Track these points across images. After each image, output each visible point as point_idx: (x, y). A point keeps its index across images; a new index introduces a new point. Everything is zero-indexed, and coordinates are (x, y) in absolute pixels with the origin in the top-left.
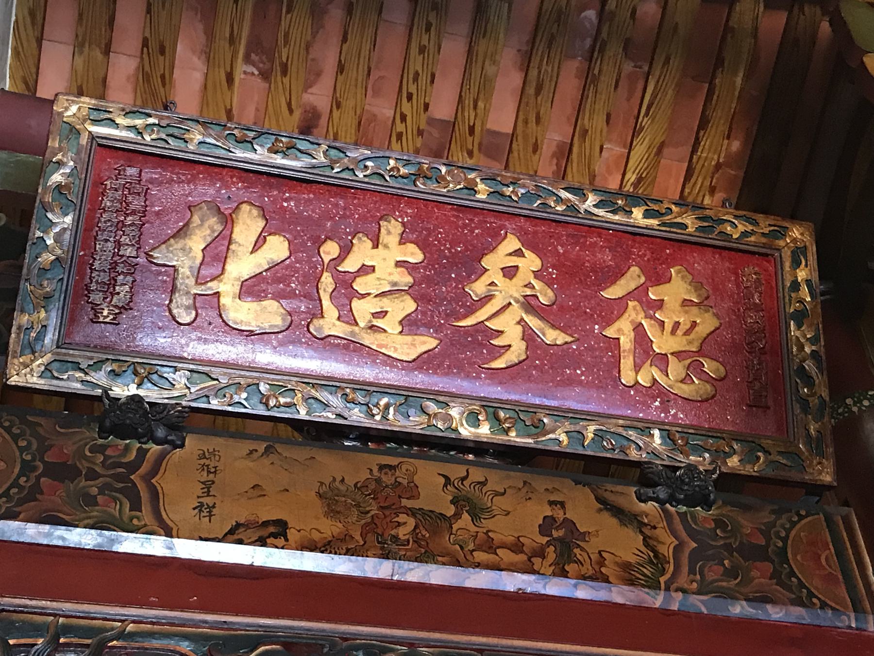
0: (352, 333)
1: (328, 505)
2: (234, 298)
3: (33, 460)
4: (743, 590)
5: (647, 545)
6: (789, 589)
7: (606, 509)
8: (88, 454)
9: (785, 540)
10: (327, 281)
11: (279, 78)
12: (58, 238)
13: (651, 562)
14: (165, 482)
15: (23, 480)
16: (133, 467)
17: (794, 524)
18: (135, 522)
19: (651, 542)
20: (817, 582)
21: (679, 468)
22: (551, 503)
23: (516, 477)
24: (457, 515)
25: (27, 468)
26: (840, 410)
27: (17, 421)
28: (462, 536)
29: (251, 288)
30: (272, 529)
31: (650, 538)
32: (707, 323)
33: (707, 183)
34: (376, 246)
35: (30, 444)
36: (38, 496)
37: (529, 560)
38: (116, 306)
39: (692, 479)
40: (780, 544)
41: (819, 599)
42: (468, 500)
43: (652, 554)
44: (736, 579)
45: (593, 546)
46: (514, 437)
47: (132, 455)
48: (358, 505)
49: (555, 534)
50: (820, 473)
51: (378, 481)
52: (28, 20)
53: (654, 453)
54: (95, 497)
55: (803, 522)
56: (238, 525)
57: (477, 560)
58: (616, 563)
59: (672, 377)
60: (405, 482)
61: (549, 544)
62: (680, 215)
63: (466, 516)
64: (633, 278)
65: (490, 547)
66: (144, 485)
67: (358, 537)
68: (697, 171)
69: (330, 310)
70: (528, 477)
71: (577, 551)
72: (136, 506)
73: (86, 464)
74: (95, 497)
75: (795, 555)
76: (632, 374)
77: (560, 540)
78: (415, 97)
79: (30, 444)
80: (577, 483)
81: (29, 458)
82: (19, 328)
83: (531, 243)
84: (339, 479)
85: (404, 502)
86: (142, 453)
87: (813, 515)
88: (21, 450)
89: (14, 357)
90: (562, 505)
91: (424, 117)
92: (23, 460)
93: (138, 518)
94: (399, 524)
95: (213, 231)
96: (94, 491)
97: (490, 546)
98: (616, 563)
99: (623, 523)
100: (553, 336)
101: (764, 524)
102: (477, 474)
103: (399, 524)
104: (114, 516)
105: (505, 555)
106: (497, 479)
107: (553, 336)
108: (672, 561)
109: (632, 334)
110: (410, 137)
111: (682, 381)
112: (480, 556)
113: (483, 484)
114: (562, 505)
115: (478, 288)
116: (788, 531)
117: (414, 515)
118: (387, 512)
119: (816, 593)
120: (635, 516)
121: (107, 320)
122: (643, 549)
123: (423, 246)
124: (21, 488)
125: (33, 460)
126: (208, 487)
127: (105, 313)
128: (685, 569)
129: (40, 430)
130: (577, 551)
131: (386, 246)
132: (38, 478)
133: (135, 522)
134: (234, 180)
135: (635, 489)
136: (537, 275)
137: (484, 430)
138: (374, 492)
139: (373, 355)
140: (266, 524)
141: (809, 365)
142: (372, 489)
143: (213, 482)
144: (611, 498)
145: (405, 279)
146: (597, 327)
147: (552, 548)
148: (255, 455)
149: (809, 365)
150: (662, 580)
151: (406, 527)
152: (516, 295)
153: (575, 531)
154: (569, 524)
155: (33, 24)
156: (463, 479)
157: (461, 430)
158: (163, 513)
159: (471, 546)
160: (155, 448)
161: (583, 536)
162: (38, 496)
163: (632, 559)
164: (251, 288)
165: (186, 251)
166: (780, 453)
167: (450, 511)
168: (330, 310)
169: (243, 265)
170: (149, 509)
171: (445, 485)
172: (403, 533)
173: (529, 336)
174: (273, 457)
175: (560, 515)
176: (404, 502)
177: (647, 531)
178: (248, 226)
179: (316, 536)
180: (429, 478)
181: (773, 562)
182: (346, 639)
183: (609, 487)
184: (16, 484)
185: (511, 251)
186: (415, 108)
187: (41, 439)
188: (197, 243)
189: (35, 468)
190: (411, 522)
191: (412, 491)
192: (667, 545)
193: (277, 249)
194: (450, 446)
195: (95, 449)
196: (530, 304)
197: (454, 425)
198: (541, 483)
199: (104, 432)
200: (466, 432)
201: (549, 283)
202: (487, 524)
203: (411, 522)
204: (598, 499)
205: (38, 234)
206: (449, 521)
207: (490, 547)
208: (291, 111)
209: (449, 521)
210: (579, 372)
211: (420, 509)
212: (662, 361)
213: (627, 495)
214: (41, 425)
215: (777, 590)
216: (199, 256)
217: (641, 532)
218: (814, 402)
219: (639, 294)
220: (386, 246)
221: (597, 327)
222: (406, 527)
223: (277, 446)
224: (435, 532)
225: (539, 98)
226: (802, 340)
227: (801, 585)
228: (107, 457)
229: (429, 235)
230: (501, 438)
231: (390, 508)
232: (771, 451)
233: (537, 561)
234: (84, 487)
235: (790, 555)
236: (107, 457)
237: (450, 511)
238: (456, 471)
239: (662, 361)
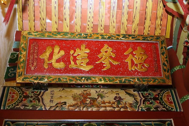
0: (77, 67)
1: (74, 98)
2: (55, 63)
3: (21, 95)
4: (153, 106)
5: (135, 99)
6: (162, 105)
7: (127, 94)
8: (31, 93)
9: (162, 96)
10: (72, 58)
11: (65, 21)
12: (23, 56)
13: (136, 103)
14: (44, 97)
15: (20, 99)
16: (39, 95)
17: (164, 93)
18: (39, 104)
19: (136, 99)
20: (168, 103)
21: (141, 85)
22: (116, 94)
23: (110, 90)
24: (98, 98)
25: (20, 97)
26: (174, 70)
27: (19, 89)
28: (99, 102)
29: (58, 61)
30: (63, 104)
31: (135, 98)
32: (144, 57)
33: (148, 30)
34: (80, 50)
35: (21, 92)
36: (22, 101)
37: (112, 105)
38: (34, 67)
39: (143, 87)
40: (161, 97)
41: (168, 106)
42: (100, 95)
43: (136, 101)
44: (152, 104)
45: (124, 101)
46: (109, 83)
47: (39, 93)
48: (79, 98)
49: (117, 99)
50: (168, 83)
51: (83, 93)
52: (20, 17)
53: (136, 83)
54: (32, 101)
55: (166, 92)
56: (57, 103)
57: (102, 106)
58: (129, 104)
59: (138, 68)
60: (88, 93)
61: (116, 101)
62: (139, 37)
63: (100, 98)
64: (130, 50)
65: (104, 103)
66: (41, 98)
67: (79, 103)
68: (145, 28)
69: (72, 63)
70: (112, 89)
71: (121, 102)
72: (39, 102)
73: (31, 95)
74: (32, 101)
75: (164, 99)
76: (131, 68)
77: (118, 100)
78: (90, 21)
79: (21, 92)
80: (122, 89)
81: (21, 95)
82: (18, 72)
83: (110, 46)
84: (76, 94)
85: (88, 97)
86: (40, 92)
87: (168, 91)
88: (20, 94)
89: (17, 78)
90: (119, 94)
91: (92, 25)
92: (20, 95)
93: (39, 104)
94: (87, 101)
95: (50, 51)
96: (32, 100)
97: (104, 103)
98: (129, 104)
99: (130, 96)
100: (115, 63)
101: (158, 93)
102: (102, 90)
103: (87, 101)
104: (35, 104)
105: (107, 104)
106: (106, 91)
107: (115, 63)
108: (140, 102)
109: (131, 61)
110: (90, 28)
111: (141, 68)
112: (102, 105)
113: (103, 92)
114: (119, 94)
115: (99, 56)
116: (163, 94)
117: (90, 99)
118: (85, 99)
119: (168, 105)
120: (133, 95)
121: (33, 69)
122: (134, 101)
123: (89, 49)
124: (19, 100)
125: (21, 95)
126: (52, 97)
127: (32, 68)
128: (142, 103)
129: (22, 90)
130: (121, 102)
131: (82, 50)
132: (22, 98)
133: (39, 104)
134: (54, 41)
135: (133, 90)
136: (112, 52)
137: (103, 82)
138: (83, 95)
139: (81, 72)
140: (62, 103)
141: (165, 63)
142: (83, 95)
143: (53, 96)
144: (128, 91)
145: (86, 55)
146: (124, 60)
147: (116, 102)
148: (61, 91)
149: (165, 63)
150: (137, 106)
151: (88, 101)
152: (108, 56)
153: (121, 98)
154: (120, 98)
155: (21, 18)
156: (100, 91)
157: (99, 82)
158: (44, 102)
159: (101, 103)
160: (43, 91)
161: (122, 99)
162: (22, 101)
163: (132, 103)
164: (58, 61)
165: (46, 55)
166: (160, 80)
167: (97, 97)
168: (72, 63)
169: (56, 57)
170: (42, 102)
171: (96, 93)
172: (88, 102)
173: (111, 63)
174: (64, 91)
175: (118, 96)
176: (88, 97)
177: (135, 97)
178: (57, 49)
179: (71, 104)
180: (93, 92)
181: (160, 100)
182: (78, 122)
183: (128, 90)
184: (18, 100)
185: (130, 52)
186: (90, 23)
187: (23, 92)
188: (48, 54)
189: (22, 97)
190: (89, 100)
191: (90, 94)
192: (139, 99)
193: (62, 53)
194: (97, 86)
195: (32, 92)
196: (111, 57)
197: (97, 82)
198: (115, 90)
199: (34, 89)
200: (100, 82)
201: (114, 53)
202: (104, 99)
203: (89, 100)
204: (126, 92)
205: (20, 56)
206: (96, 99)
207: (104, 103)
208: (68, 27)
209: (96, 99)
210: (121, 69)
211: (91, 97)
212: (136, 65)
213: (131, 91)
214: (23, 89)
215: (160, 106)
216: (48, 56)
217: (134, 97)
218: (167, 70)
219: (132, 53)
220: (82, 50)
221: (124, 60)
222: (88, 101)
223: (64, 88)
224: (94, 101)
225: (113, 18)
226: (164, 58)
227: (165, 104)
228: (34, 94)
229: (91, 47)
230: (106, 83)
231: (85, 98)
232: (159, 79)
233: (113, 105)
234: (30, 99)
235: (163, 99)
236: (34, 94)
237: (97, 97)
238: (98, 90)
239: (136, 65)
